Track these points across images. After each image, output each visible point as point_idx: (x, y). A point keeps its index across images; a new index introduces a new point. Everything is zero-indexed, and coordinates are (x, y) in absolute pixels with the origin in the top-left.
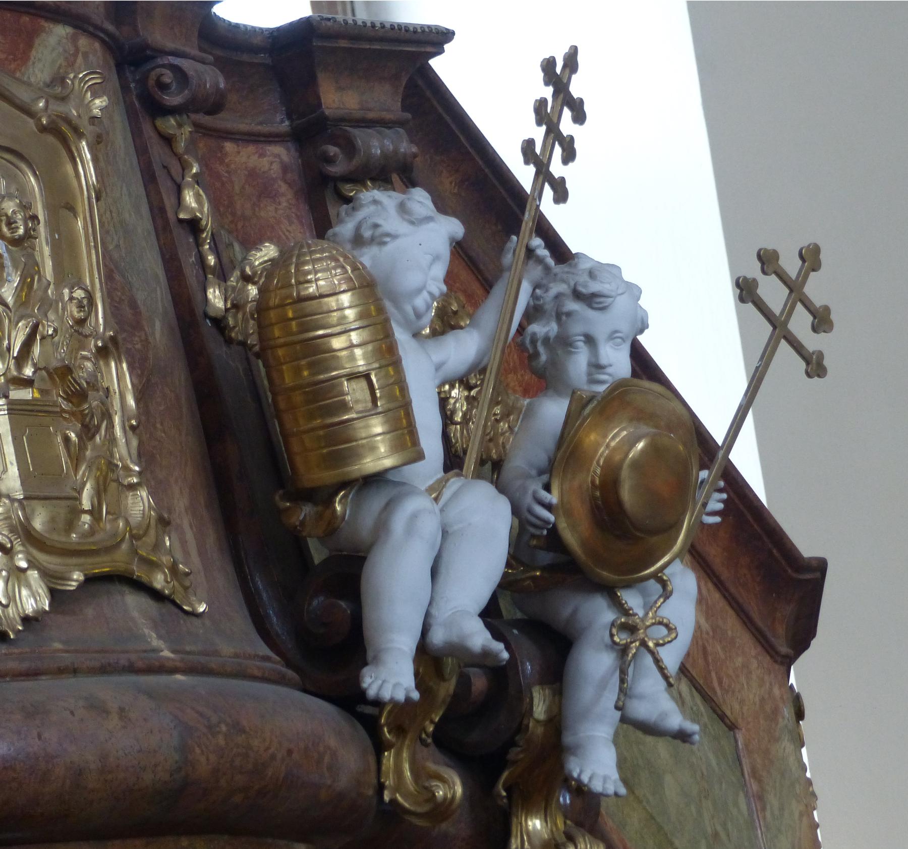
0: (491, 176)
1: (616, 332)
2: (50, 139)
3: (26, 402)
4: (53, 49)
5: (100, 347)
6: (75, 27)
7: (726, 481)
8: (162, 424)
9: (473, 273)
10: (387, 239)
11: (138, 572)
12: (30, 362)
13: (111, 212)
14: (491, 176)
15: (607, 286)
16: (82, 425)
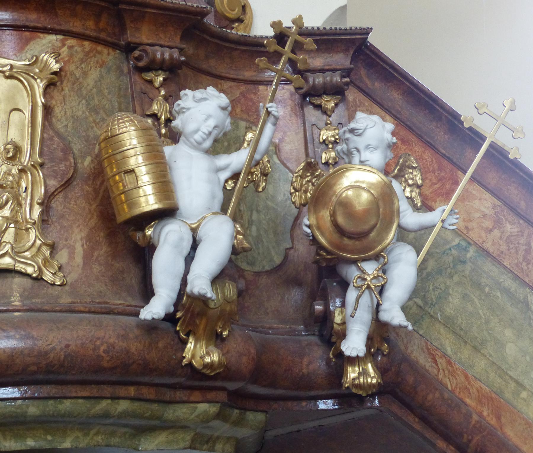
0: (415, 89)
1: (369, 145)
2: (15, 82)
4: (44, 45)
8: (75, 202)
10: (185, 110)
11: (19, 267)
13: (66, 112)
14: (415, 89)
15: (361, 125)
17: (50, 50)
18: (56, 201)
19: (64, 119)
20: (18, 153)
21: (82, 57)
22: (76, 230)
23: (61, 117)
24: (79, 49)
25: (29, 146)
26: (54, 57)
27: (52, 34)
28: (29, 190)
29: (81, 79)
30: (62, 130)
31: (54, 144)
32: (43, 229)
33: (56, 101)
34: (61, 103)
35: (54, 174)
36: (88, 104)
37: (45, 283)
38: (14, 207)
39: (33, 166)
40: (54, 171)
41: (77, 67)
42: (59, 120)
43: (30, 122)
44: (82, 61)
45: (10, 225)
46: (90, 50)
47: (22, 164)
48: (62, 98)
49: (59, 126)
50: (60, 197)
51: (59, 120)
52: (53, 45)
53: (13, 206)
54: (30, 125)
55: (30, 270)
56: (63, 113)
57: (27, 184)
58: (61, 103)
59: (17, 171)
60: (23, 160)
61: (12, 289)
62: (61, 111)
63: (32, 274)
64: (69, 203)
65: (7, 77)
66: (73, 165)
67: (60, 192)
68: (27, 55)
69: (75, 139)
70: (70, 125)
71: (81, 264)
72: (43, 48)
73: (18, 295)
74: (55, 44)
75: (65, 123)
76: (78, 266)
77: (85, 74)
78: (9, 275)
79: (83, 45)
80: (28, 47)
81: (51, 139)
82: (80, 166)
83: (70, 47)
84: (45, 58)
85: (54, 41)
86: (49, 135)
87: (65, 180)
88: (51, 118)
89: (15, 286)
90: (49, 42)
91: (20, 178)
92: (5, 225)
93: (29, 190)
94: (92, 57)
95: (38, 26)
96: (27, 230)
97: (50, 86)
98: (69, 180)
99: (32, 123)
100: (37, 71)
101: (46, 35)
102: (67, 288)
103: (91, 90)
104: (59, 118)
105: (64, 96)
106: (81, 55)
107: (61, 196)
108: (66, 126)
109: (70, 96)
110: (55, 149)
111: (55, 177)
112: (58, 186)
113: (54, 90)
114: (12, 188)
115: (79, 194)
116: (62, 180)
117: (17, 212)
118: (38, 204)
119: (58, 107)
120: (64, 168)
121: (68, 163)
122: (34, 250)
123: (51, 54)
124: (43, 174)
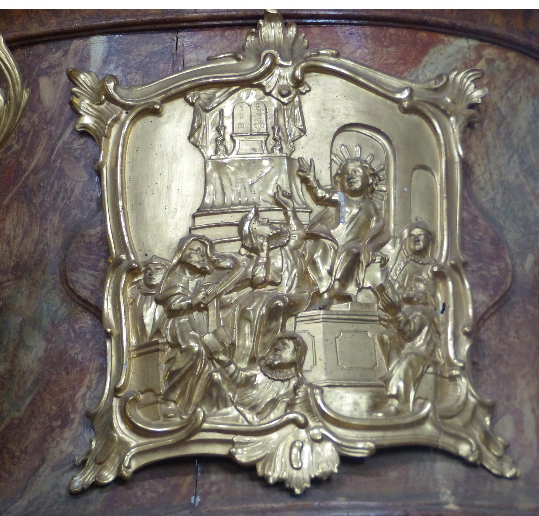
2: (416, 118)
3: (344, 313)
4: (450, 56)
5: (436, 272)
6: (480, 40)
7: (292, 367)
8: (517, 332)
9: (28, 163)
11: (445, 442)
12: (354, 283)
13: (491, 174)
16: (398, 329)
17: (459, 65)
18: (487, 329)
19: (489, 186)
20: (430, 244)
21: (507, 79)
22: (522, 383)
23: (485, 182)
24: (501, 65)
25: (446, 233)
26: (472, 79)
27: (461, 36)
28: (451, 309)
29: (509, 118)
30: (488, 206)
31: (480, 231)
32: (474, 376)
33: (476, 156)
34: (483, 159)
35: (483, 283)
36: (522, 162)
37: (486, 474)
38: (431, 339)
39: (454, 266)
40: (482, 277)
41: (502, 97)
42: (482, 189)
43: (444, 190)
44: (509, 86)
45: (428, 367)
46: (518, 66)
47: (436, 263)
48: (484, 150)
49: (483, 199)
50: (492, 323)
51: (482, 189)
52: (464, 57)
53: (429, 337)
54: (445, 195)
55: (464, 449)
56: (487, 176)
57: (446, 297)
58: (483, 159)
59: (430, 274)
60: (437, 257)
61: (435, 481)
62: (484, 173)
63: (468, 456)
64: (507, 334)
65: (406, 111)
66: (510, 268)
67: (492, 314)
68: (426, 72)
69: (508, 223)
70: (499, 197)
71: (535, 441)
72: (449, 60)
73: (449, 492)
74: (467, 56)
75: (491, 194)
76: (531, 445)
77: (514, 108)
78: (425, 456)
79: (507, 59)
80: (427, 58)
81: (474, 221)
82: (519, 270)
83: (490, 62)
84: (459, 78)
85: (465, 50)
86: (470, 213)
87: (501, 293)
88: (470, 184)
89: (439, 477)
90: (458, 52)
91: (436, 287)
92: (421, 368)
93: (451, 309)
94: (520, 80)
95: (442, 23)
96: (453, 378)
97: (469, 127)
98: (506, 293)
99: (448, 192)
100: (449, 100)
101: (452, 39)
102: (521, 483)
103: (525, 137)
104: (482, 184)
105: (487, 147)
106: (504, 77)
107: (494, 322)
108: (493, 200)
109: (495, 147)
110: (481, 239)
111: (485, 288)
112: (491, 304)
113: (471, 135)
114: (426, 304)
115: (520, 320)
116: (496, 293)
117: (435, 346)
118: (466, 333)
119: (479, 165)
120: (496, 273)
121: (503, 265)
122: (467, 414)
123: (468, 72)
124: (470, 284)
